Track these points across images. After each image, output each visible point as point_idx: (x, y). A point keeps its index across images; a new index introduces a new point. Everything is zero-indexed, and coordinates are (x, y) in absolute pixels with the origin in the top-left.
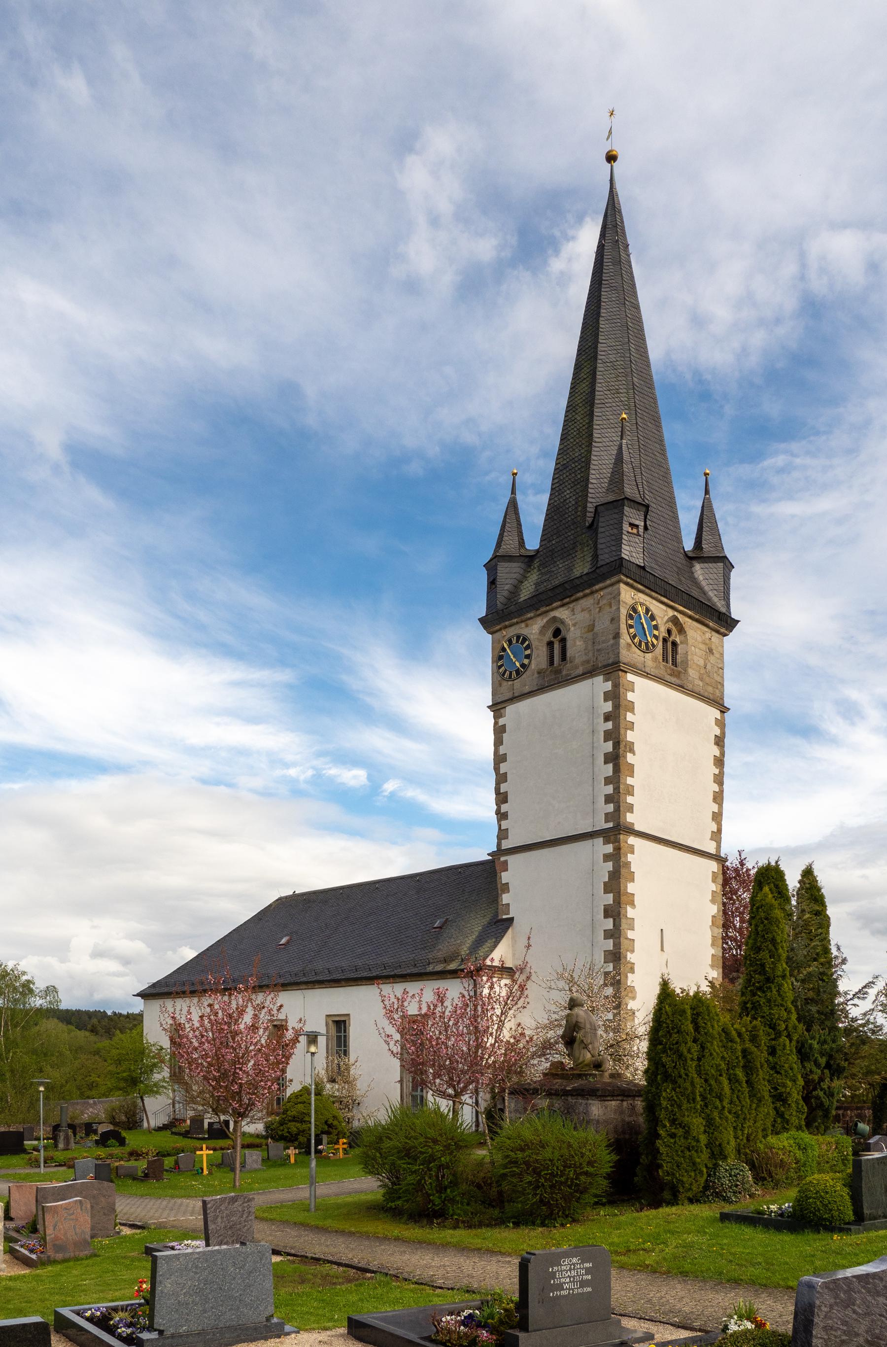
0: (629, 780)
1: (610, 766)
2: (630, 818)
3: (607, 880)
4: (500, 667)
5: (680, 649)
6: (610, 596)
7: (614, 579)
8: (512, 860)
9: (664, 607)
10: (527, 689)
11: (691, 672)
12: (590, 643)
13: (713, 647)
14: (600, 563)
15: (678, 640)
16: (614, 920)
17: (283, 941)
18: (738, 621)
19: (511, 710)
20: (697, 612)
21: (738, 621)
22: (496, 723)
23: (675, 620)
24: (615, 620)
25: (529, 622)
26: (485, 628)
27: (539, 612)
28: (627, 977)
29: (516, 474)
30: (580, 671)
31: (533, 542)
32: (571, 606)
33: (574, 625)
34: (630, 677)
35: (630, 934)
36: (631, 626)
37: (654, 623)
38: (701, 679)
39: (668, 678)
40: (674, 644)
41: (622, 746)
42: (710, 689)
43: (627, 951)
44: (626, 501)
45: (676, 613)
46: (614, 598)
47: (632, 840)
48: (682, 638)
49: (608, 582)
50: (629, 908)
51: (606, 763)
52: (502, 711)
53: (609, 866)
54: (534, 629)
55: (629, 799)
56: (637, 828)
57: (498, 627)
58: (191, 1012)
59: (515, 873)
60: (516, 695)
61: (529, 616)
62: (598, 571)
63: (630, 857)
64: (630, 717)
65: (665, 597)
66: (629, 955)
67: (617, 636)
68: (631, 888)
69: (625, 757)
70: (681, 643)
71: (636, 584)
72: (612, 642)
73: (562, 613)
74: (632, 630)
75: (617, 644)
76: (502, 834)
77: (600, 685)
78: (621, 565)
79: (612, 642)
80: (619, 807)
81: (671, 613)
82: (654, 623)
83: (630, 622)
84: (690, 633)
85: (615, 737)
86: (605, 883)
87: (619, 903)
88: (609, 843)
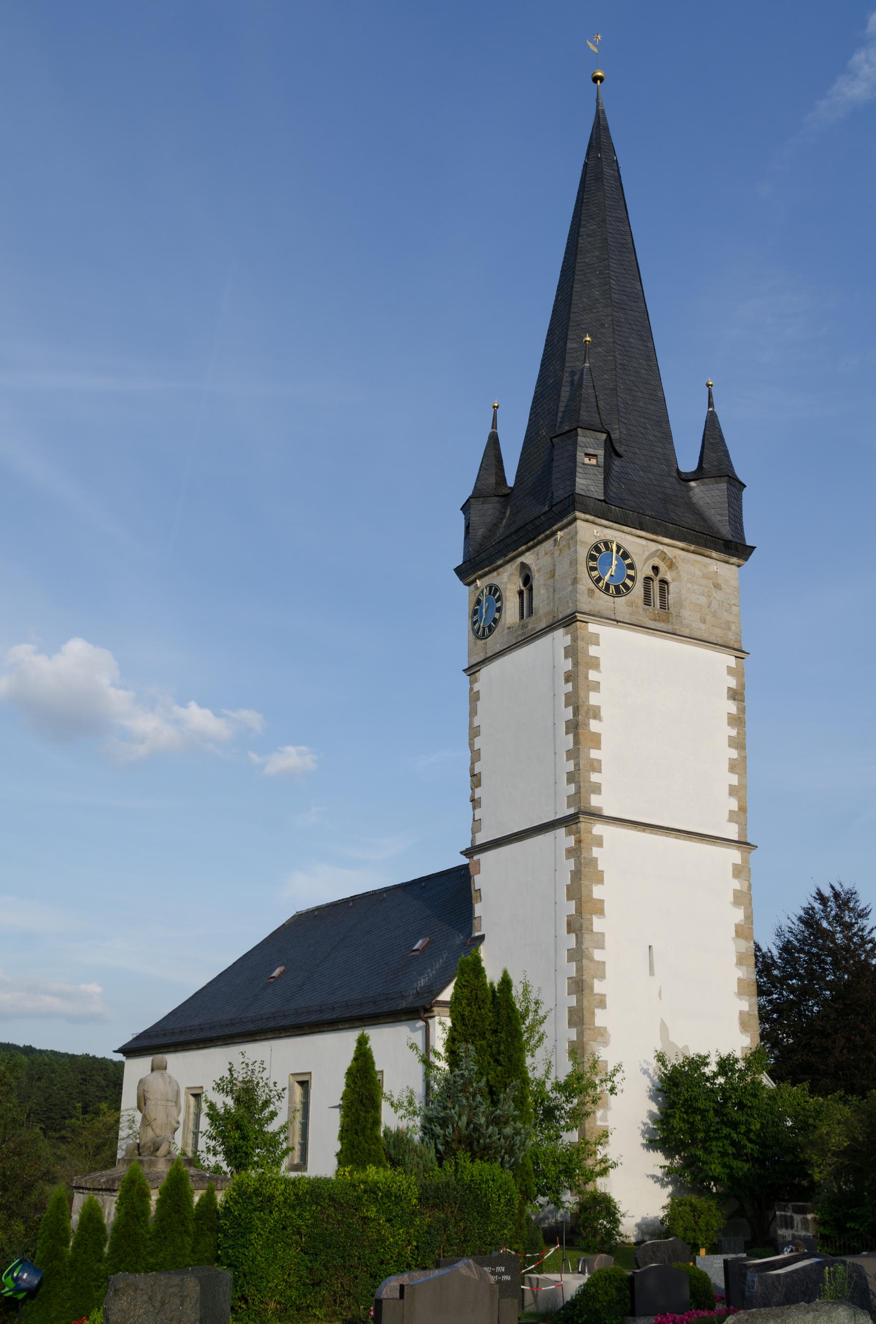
0: (594, 754)
1: (571, 737)
2: (595, 801)
3: (569, 883)
4: (474, 623)
5: (672, 587)
6: (568, 537)
7: (570, 518)
8: (485, 858)
9: (643, 542)
10: (498, 648)
11: (686, 613)
12: (551, 590)
13: (720, 581)
14: (556, 501)
15: (668, 578)
16: (577, 935)
17: (276, 973)
18: (754, 548)
19: (485, 672)
20: (691, 542)
21: (754, 548)
22: (471, 689)
23: (664, 557)
24: (574, 562)
25: (501, 570)
26: (461, 579)
27: (507, 558)
28: (593, 1014)
29: (497, 407)
30: (543, 625)
31: (511, 481)
32: (536, 549)
33: (539, 571)
34: (593, 628)
35: (598, 955)
36: (593, 569)
37: (628, 561)
38: (703, 621)
39: (652, 624)
40: (663, 582)
41: (582, 712)
42: (718, 631)
43: (593, 978)
44: (579, 430)
45: (661, 547)
46: (572, 538)
47: (599, 829)
48: (674, 574)
49: (565, 521)
50: (595, 920)
51: (567, 733)
52: (477, 674)
53: (571, 864)
54: (507, 579)
55: (594, 777)
56: (606, 813)
57: (472, 578)
58: (201, 1070)
59: (491, 877)
60: (488, 655)
61: (499, 562)
62: (554, 509)
63: (596, 852)
64: (593, 675)
65: (642, 529)
66: (596, 983)
67: (575, 581)
68: (598, 892)
69: (588, 725)
70: (673, 580)
71: (598, 520)
72: (570, 588)
73: (528, 558)
74: (594, 573)
75: (575, 591)
76: (476, 825)
77: (560, 638)
78: (574, 502)
79: (570, 588)
80: (580, 787)
81: (653, 547)
82: (628, 561)
83: (591, 564)
84: (682, 567)
85: (574, 701)
86: (568, 887)
87: (581, 913)
88: (570, 834)
